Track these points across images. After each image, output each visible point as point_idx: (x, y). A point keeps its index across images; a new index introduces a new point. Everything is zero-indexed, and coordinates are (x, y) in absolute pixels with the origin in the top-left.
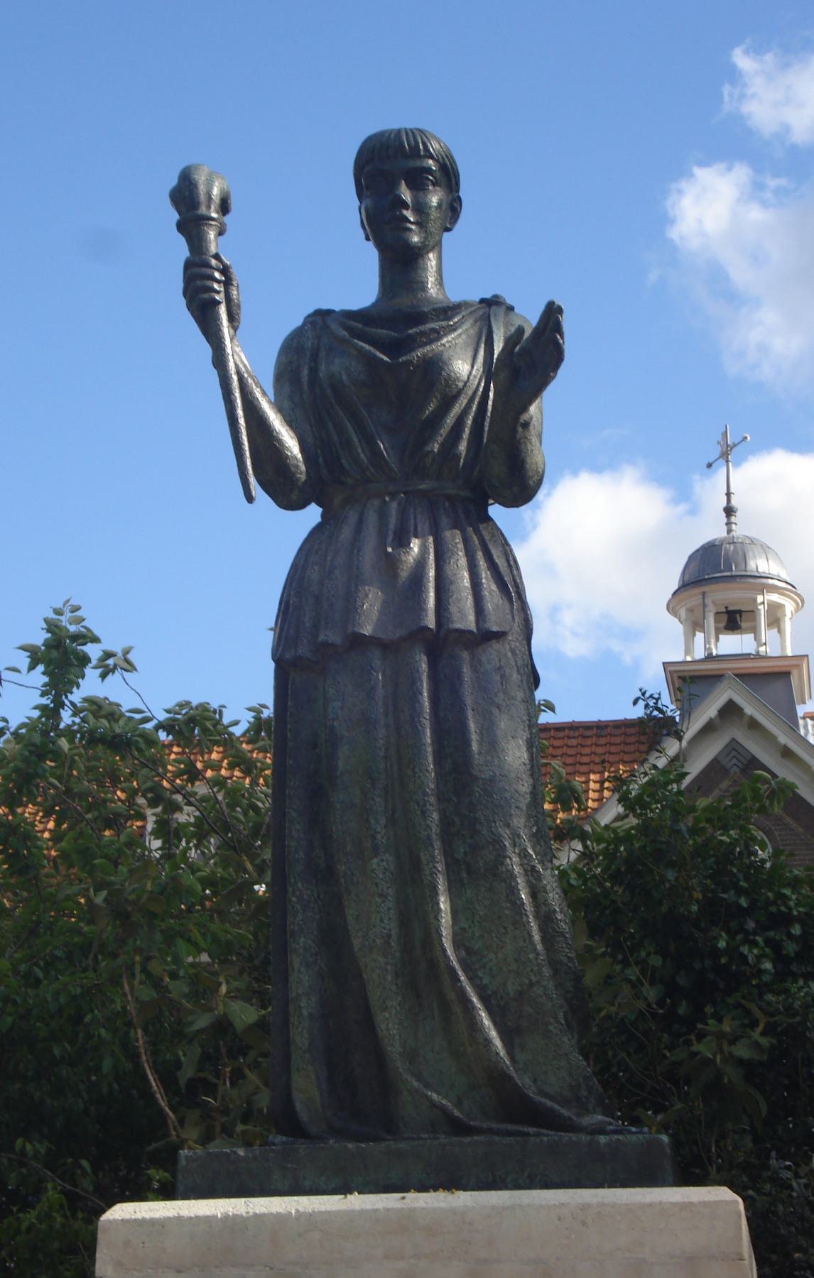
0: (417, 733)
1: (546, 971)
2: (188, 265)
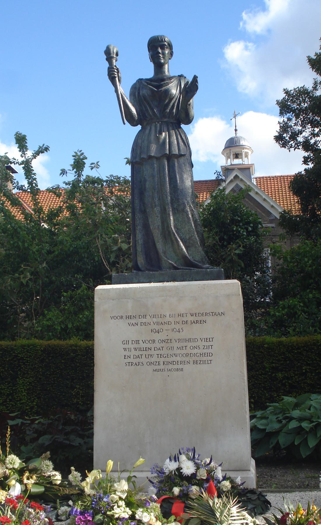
0: (165, 179)
1: (195, 233)
2: (109, 68)
